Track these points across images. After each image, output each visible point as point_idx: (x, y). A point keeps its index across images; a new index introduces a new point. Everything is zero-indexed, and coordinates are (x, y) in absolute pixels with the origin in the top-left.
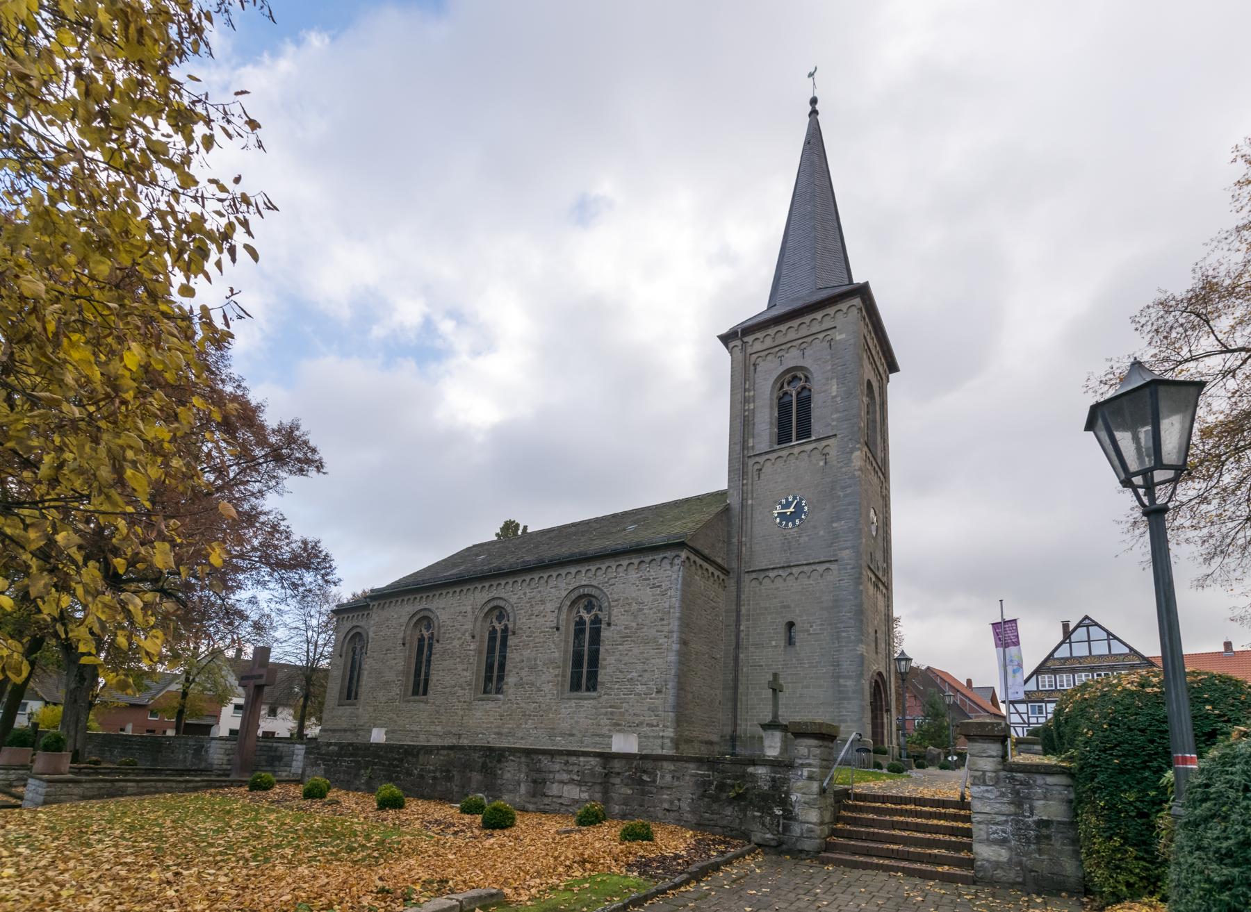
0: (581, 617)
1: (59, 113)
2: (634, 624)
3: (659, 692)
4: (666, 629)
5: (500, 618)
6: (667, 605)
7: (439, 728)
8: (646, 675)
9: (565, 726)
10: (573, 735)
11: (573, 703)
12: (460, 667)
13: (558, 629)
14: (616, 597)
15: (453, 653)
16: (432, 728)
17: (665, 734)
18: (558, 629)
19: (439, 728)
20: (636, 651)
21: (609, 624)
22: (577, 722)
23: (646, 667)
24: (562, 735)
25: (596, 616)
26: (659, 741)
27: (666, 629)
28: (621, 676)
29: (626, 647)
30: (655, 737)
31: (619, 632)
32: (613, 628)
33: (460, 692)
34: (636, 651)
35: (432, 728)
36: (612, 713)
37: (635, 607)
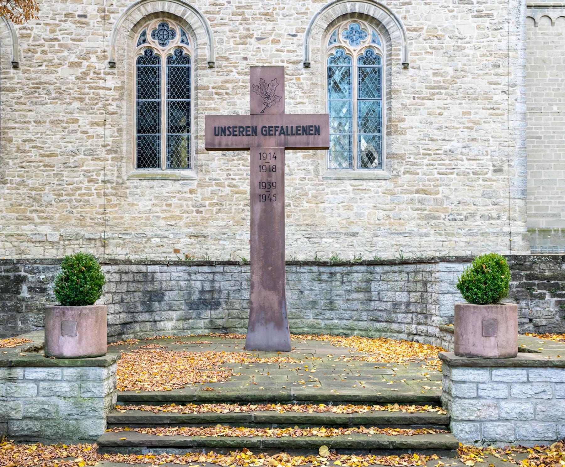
0: (149, 51)
1: (348, 361)
2: (450, 70)
3: (498, 170)
4: (504, 80)
5: (164, 33)
6: (503, 45)
7: (45, 229)
8: (476, 147)
9: (335, 221)
10: (355, 234)
11: (347, 185)
12: (84, 120)
13: (307, 65)
14: (415, 24)
15: (59, 91)
16: (28, 229)
17: (513, 229)
18: (307, 65)
19: (45, 229)
20: (456, 110)
21: (405, 66)
22: (359, 215)
23: (474, 134)
24: (334, 235)
25: (179, 51)
26: (506, 239)
27: (504, 80)
28: (432, 145)
29: (441, 103)
30: (497, 234)
31: (425, 79)
32: (411, 71)
33: (91, 165)
34: (456, 110)
35: (28, 229)
36: (421, 202)
37: (448, 43)
